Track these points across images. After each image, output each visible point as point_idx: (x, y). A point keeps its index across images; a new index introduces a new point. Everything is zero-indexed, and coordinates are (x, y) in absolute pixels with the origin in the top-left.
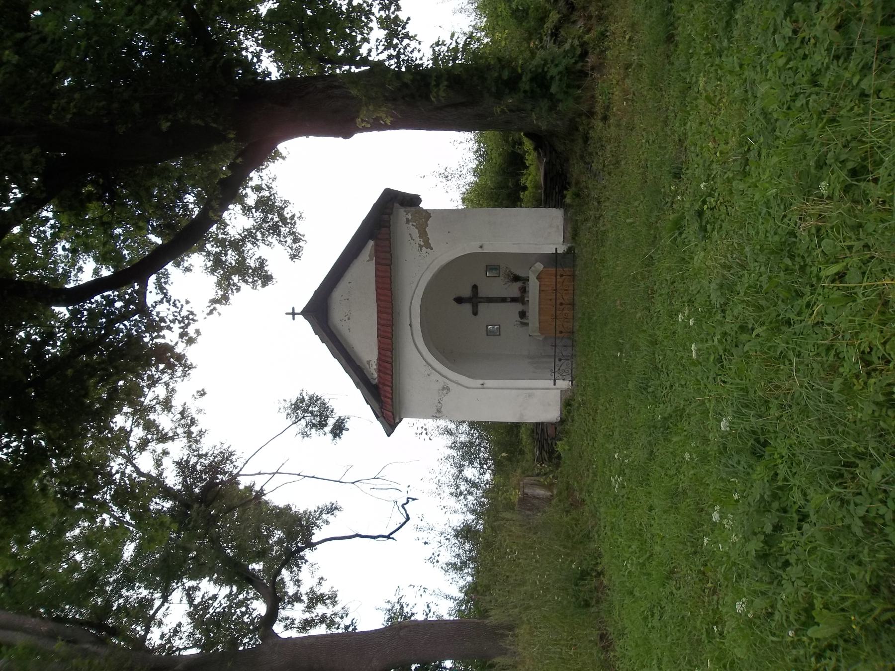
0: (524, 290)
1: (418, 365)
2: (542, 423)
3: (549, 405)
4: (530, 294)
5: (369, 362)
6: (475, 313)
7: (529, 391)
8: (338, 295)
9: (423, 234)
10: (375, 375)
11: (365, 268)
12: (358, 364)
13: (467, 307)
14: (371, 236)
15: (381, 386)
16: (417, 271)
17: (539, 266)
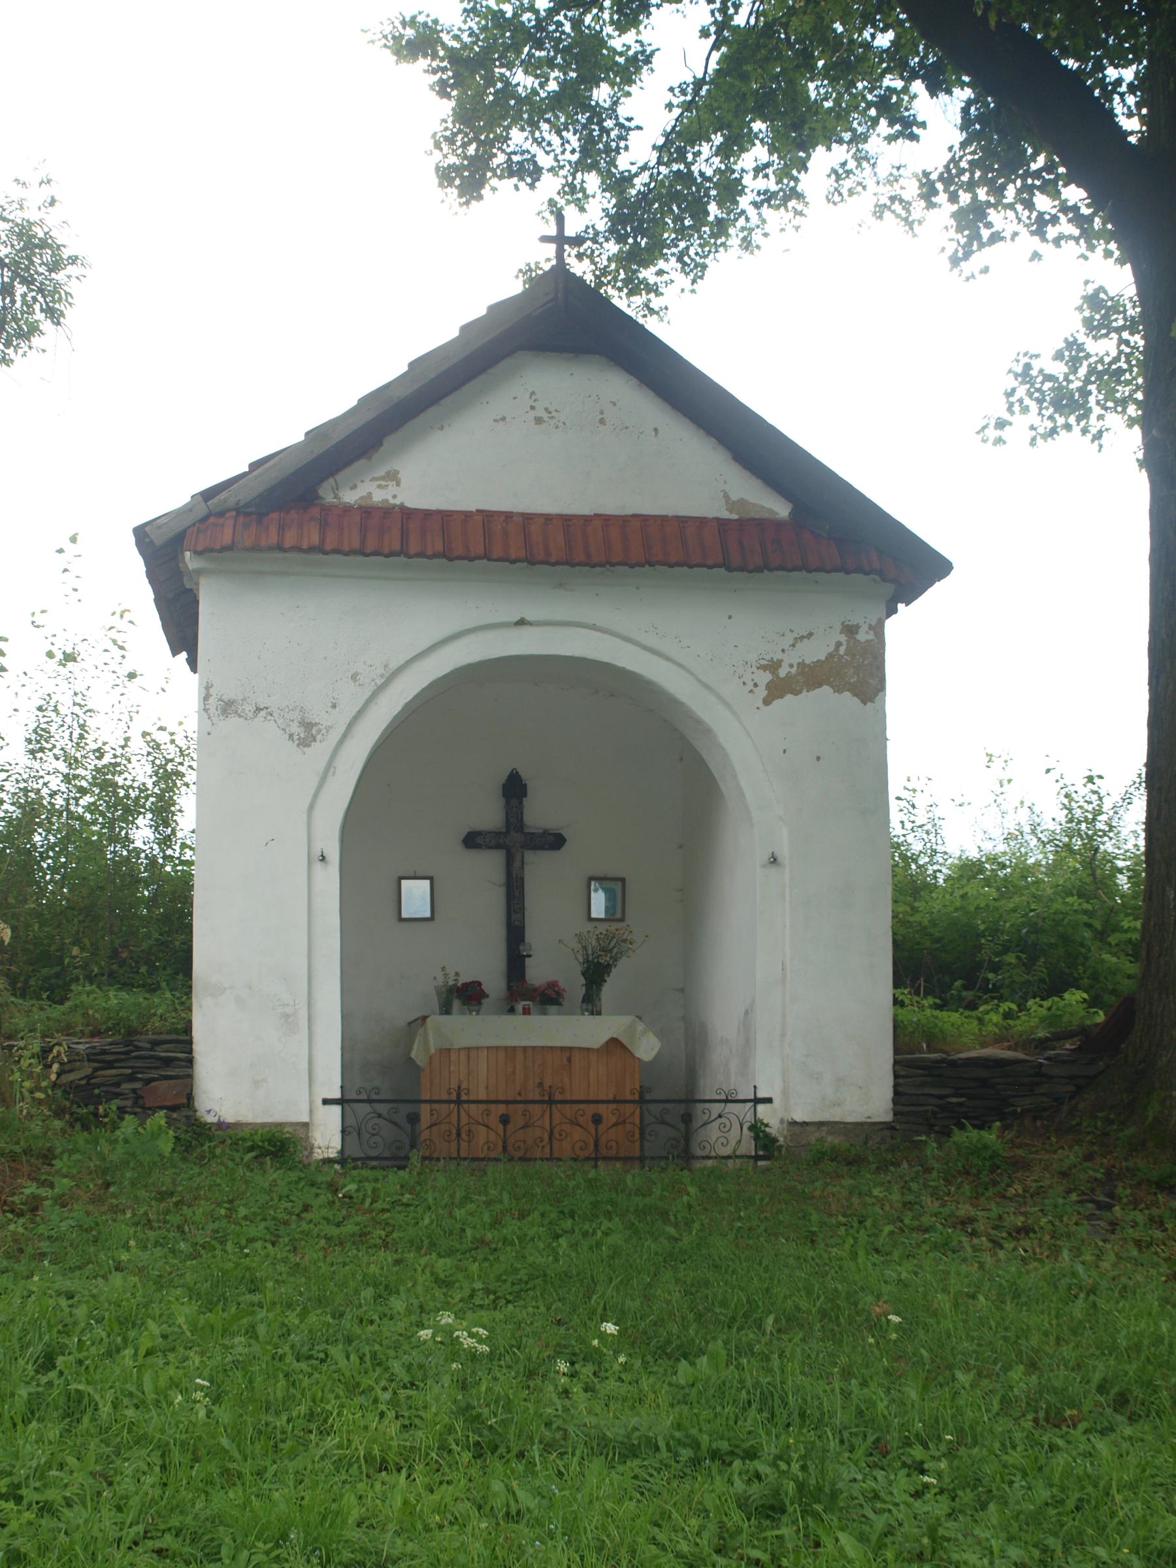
0: (548, 998)
1: (378, 649)
2: (190, 1062)
3: (257, 1084)
4: (535, 1020)
5: (393, 476)
6: (472, 841)
7: (303, 1013)
8: (616, 389)
9: (811, 677)
10: (350, 497)
11: (698, 483)
12: (389, 441)
13: (490, 816)
14: (801, 509)
15: (315, 512)
16: (691, 651)
17: (647, 1048)
